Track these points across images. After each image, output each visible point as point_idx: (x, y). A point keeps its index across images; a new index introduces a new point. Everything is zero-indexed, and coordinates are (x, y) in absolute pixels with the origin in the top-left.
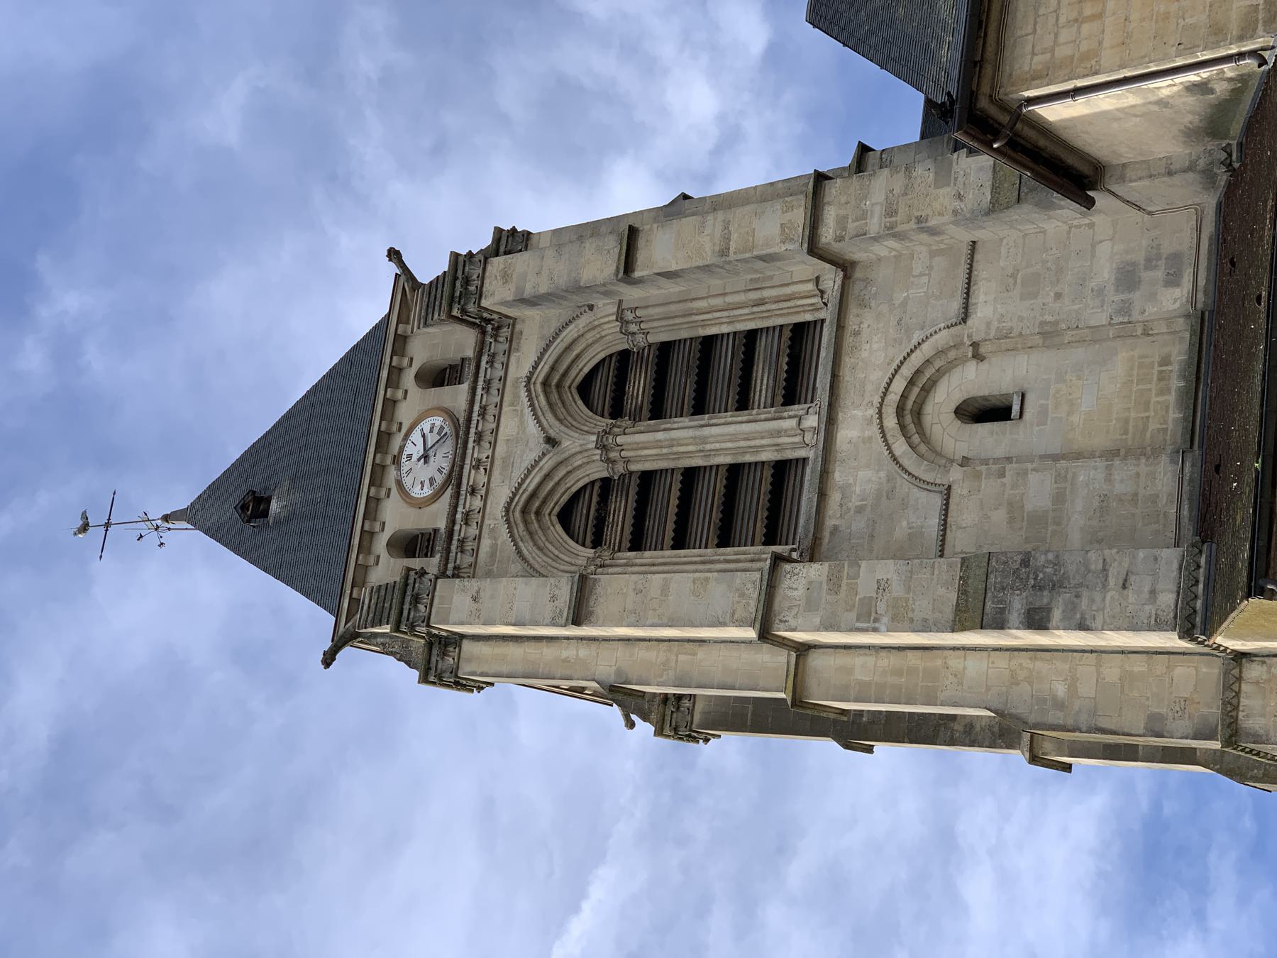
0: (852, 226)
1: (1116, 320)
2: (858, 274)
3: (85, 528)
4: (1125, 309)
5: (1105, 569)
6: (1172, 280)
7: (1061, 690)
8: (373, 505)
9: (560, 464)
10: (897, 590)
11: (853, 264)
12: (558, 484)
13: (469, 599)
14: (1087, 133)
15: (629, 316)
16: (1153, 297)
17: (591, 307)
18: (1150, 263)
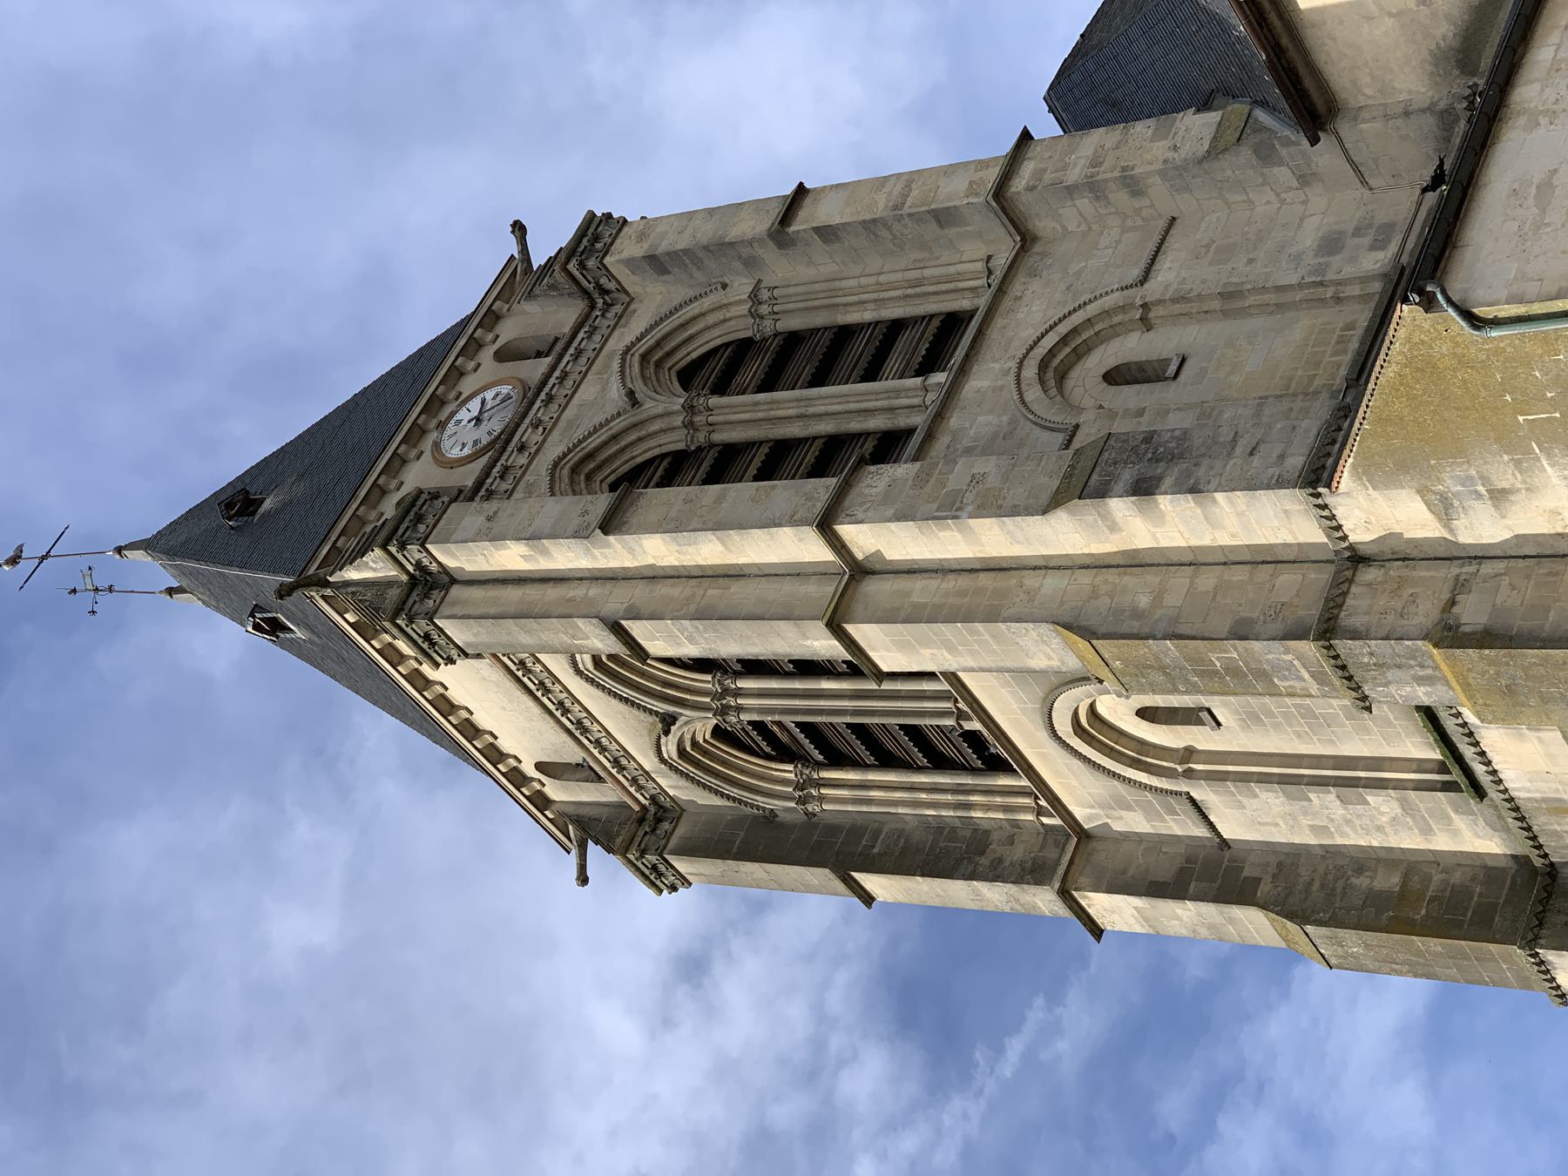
1: (1308, 280)
2: (1037, 248)
3: (14, 561)
5: (1234, 441)
7: (1144, 601)
8: (397, 463)
9: (635, 426)
11: (1035, 239)
12: (623, 450)
13: (482, 518)
14: (1334, 39)
16: (1353, 259)
17: (724, 286)
18: (1358, 232)
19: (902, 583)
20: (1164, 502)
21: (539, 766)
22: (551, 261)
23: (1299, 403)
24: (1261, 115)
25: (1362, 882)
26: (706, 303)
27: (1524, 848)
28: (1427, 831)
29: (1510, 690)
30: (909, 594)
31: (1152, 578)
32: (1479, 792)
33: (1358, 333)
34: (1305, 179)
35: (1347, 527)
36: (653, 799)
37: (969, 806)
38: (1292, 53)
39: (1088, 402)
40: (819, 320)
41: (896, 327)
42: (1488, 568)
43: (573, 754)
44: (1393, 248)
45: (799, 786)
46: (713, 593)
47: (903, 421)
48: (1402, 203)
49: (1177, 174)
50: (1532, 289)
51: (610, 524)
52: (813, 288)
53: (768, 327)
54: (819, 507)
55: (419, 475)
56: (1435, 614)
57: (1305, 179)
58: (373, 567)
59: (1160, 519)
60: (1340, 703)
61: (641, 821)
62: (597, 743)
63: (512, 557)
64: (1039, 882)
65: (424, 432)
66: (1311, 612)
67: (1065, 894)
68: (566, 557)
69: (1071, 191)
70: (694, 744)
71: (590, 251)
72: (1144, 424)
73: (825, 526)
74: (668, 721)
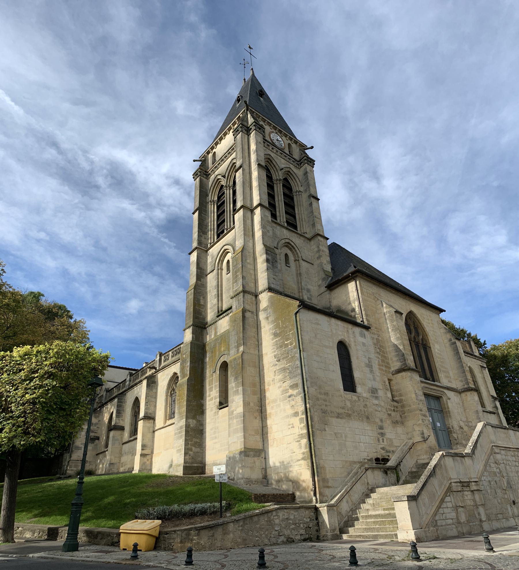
0: (321, 243)
2: (308, 241)
3: (250, 47)
4: (304, 289)
7: (248, 261)
15: (300, 193)
18: (310, 295)
19: (250, 218)
20: (265, 264)
21: (215, 152)
24: (330, 278)
25: (202, 298)
26: (299, 183)
28: (211, 308)
29: (235, 321)
31: (252, 262)
32: (218, 317)
33: (294, 295)
34: (319, 286)
36: (210, 174)
39: (282, 251)
40: (296, 203)
41: (295, 217)
42: (255, 317)
45: (213, 201)
47: (278, 218)
49: (321, 265)
51: (259, 165)
52: (301, 202)
53: (294, 194)
54: (263, 203)
55: (267, 129)
56: (247, 309)
58: (250, 120)
60: (232, 294)
61: (206, 172)
62: (220, 163)
63: (253, 147)
65: (275, 130)
66: (247, 289)
67: (196, 248)
68: (253, 157)
69: (318, 247)
71: (308, 161)
72: (278, 261)
73: (260, 205)
74: (224, 177)
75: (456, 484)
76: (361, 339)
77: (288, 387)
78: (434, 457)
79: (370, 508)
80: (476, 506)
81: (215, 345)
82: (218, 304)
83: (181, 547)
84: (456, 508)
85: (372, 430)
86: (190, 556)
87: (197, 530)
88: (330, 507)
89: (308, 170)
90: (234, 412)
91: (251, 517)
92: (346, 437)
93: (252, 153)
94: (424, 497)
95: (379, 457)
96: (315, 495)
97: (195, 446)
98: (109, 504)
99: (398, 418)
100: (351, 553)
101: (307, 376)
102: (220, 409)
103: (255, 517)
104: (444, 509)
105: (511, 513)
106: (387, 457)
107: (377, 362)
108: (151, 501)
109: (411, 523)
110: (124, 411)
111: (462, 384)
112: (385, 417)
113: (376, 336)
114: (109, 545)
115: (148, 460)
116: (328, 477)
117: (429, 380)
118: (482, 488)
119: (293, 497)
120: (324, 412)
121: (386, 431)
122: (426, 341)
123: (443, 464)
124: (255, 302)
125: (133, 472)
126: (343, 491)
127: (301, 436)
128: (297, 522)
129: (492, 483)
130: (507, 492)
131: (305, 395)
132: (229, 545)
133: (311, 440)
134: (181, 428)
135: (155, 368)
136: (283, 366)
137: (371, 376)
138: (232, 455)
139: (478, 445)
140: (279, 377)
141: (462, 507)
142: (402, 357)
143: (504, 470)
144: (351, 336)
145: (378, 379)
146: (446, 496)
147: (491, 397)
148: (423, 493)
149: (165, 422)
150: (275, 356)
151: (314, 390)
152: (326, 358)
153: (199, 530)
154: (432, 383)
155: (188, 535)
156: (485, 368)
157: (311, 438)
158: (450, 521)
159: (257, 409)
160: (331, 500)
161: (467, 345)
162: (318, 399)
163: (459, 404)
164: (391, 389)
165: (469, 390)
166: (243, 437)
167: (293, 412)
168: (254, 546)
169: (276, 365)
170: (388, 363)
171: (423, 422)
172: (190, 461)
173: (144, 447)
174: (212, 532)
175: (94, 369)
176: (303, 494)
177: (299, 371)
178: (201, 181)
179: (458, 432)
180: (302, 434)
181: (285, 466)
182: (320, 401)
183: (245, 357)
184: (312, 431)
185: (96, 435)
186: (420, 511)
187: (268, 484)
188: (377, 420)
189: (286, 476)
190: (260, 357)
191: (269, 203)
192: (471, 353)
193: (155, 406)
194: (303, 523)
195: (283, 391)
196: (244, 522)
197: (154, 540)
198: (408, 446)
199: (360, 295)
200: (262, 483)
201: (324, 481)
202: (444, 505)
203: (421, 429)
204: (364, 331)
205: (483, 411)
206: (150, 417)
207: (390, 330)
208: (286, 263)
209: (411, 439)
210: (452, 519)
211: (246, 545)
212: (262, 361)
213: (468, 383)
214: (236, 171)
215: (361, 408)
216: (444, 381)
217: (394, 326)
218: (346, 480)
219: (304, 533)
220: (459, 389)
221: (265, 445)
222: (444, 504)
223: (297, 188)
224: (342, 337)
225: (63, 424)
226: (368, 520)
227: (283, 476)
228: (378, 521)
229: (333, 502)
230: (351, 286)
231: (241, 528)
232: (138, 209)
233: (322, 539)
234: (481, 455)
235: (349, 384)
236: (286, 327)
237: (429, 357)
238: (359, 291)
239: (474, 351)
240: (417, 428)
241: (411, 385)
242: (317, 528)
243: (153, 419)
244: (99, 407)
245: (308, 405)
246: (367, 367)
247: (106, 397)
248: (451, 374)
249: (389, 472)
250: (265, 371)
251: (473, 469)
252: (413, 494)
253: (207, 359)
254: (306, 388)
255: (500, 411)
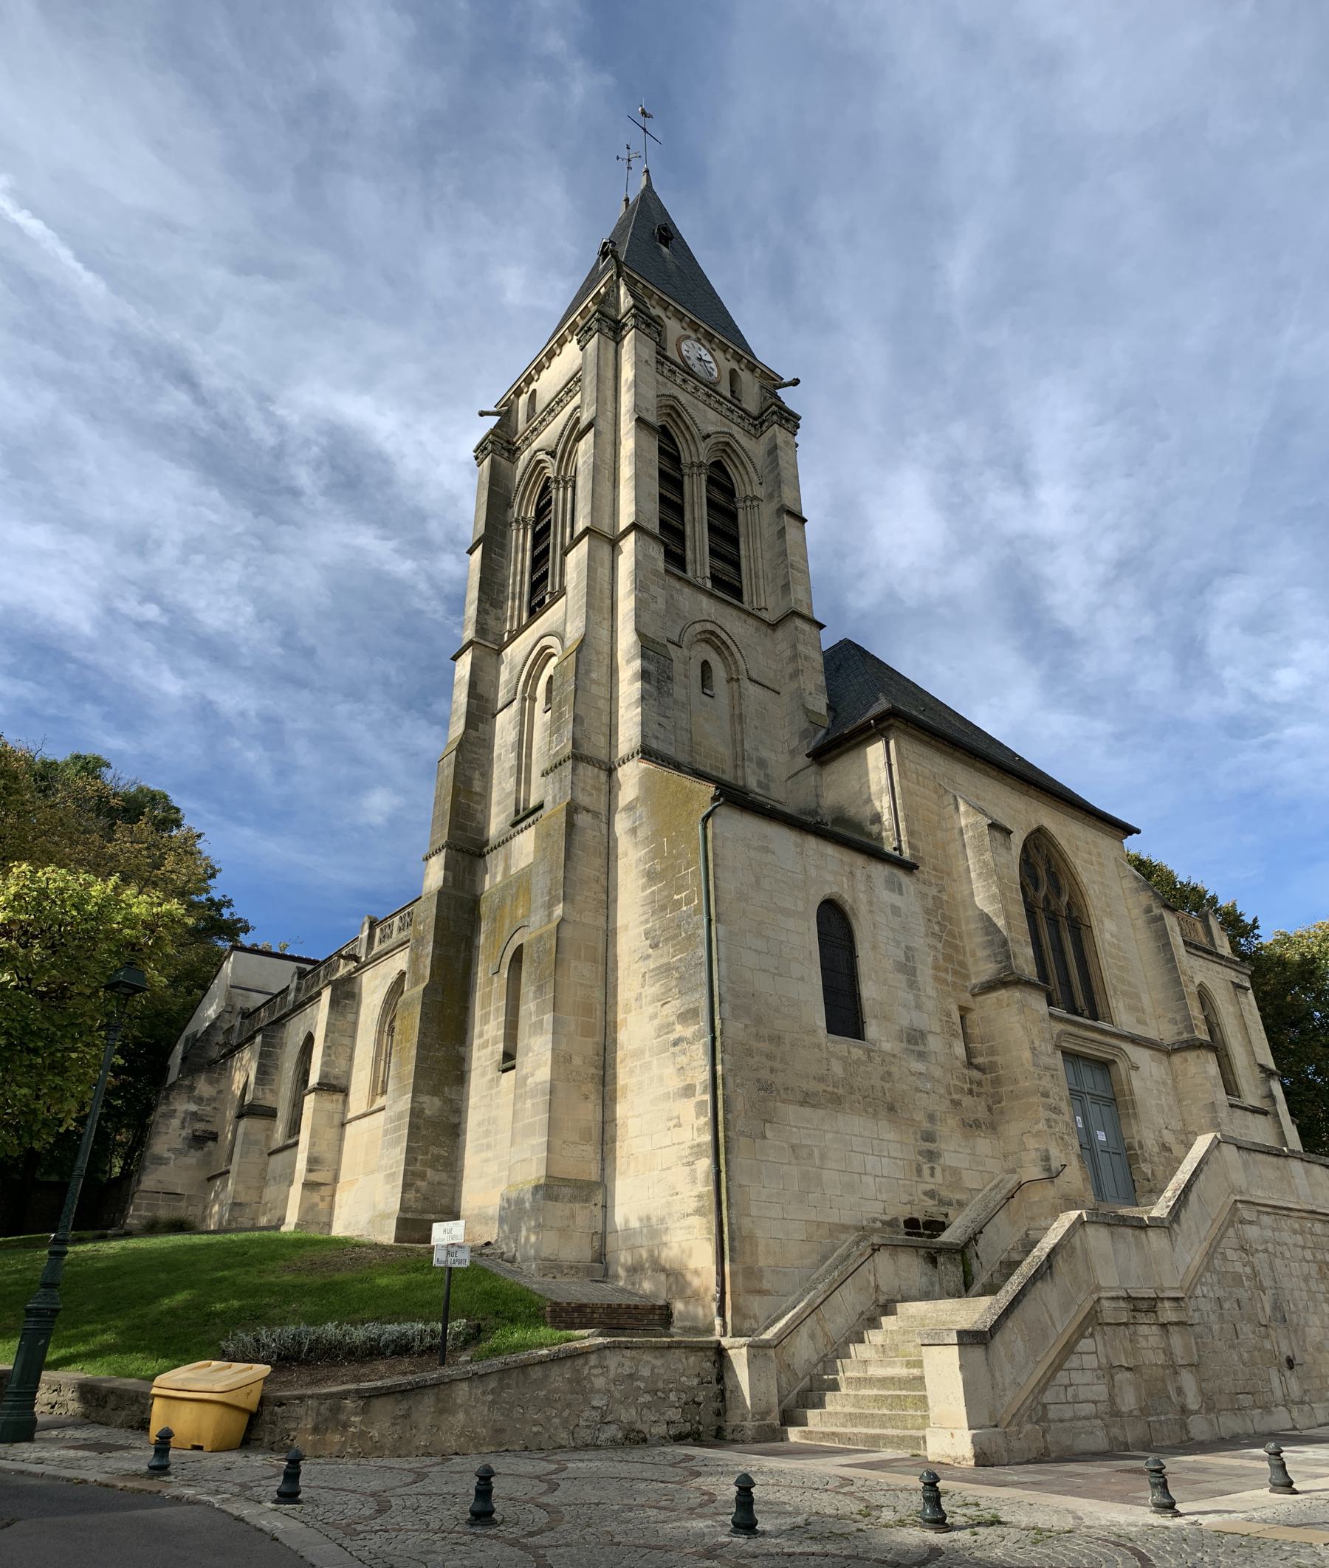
3: (644, 113)
4: (750, 759)
6: (759, 784)
7: (594, 675)
10: (653, 606)
15: (755, 503)
18: (766, 775)
19: (607, 564)
20: (638, 685)
21: (534, 391)
22: (779, 398)
23: (687, 748)
24: (823, 732)
25: (477, 775)
26: (753, 475)
27: (491, 844)
28: (499, 803)
29: (549, 835)
30: (602, 566)
31: (605, 679)
32: (514, 825)
33: (720, 775)
34: (793, 753)
35: (624, 767)
36: (519, 448)
37: (513, 600)
38: (848, 745)
39: (693, 653)
40: (742, 530)
41: (737, 566)
42: (604, 827)
43: (539, 408)
44: (758, 790)
45: (524, 519)
46: (607, 473)
47: (689, 567)
48: (782, 795)
49: (799, 694)
50: (719, 843)
51: (640, 421)
52: (756, 526)
53: (741, 504)
54: (644, 524)
55: (673, 328)
56: (583, 804)
57: (793, 753)
58: (625, 301)
59: (631, 683)
60: (547, 765)
61: (508, 442)
62: (544, 420)
63: (627, 373)
64: (477, 631)
65: (696, 331)
66: (585, 750)
67: (471, 643)
68: (626, 400)
69: (794, 647)
70: (544, 468)
71: (782, 417)
72: (677, 678)
73: (634, 527)
74: (552, 454)
75: (1113, 1304)
76: (887, 897)
77: (673, 1018)
78: (1055, 1225)
79: (870, 1359)
80: (1174, 1369)
81: (502, 901)
82: (518, 791)
83: (314, 1444)
84: (1110, 1371)
85: (902, 1143)
86: (292, 1474)
87: (361, 1398)
88: (757, 1350)
89: (780, 441)
90: (530, 1081)
91: (524, 1367)
92: (823, 1157)
93: (624, 389)
94: (1013, 1334)
95: (916, 1215)
96: (721, 1312)
97: (433, 1167)
98: (172, 1312)
99: (981, 1113)
100: (738, 1494)
101: (724, 989)
102: (504, 1071)
103: (537, 1368)
104: (1073, 1374)
105: (1278, 1393)
106: (941, 1219)
107: (930, 959)
108: (277, 1311)
109: (964, 1410)
110: (276, 1067)
111: (1175, 1029)
112: (942, 1107)
113: (934, 891)
114: (131, 1427)
115: (322, 1199)
116: (762, 1263)
117: (1081, 1015)
118: (1196, 1318)
119: (664, 1315)
120: (766, 1088)
121: (943, 1146)
122: (1080, 911)
123: (1078, 1244)
124: (605, 788)
125: (283, 1229)
126: (802, 1304)
127: (697, 1150)
128: (661, 1385)
129: (1227, 1305)
130: (1272, 1333)
131: (714, 1039)
132: (452, 1443)
133: (722, 1162)
134: (400, 1116)
135: (356, 959)
136: (664, 961)
137: (911, 997)
138: (514, 1195)
139: (1193, 1197)
140: (654, 990)
141: (1128, 1369)
142: (1001, 947)
143: (1267, 1270)
144: (862, 887)
145: (930, 1005)
146: (1082, 1336)
147: (1257, 1070)
148: (1010, 1324)
149: (372, 1102)
150: (647, 934)
151: (741, 1026)
152: (782, 942)
153: (368, 1397)
154: (1089, 1022)
155: (336, 1410)
156: (1247, 989)
157: (722, 1157)
158: (1088, 1409)
159: (592, 1075)
160: (767, 1328)
161: (1199, 925)
162: (749, 1053)
163: (1164, 1083)
164: (965, 1033)
165: (1200, 1046)
166: (545, 1146)
167: (682, 1084)
168: (526, 1449)
169: (649, 956)
170: (963, 964)
171: (1050, 1127)
172: (419, 1206)
173: (313, 1163)
174: (405, 1405)
175: (133, 946)
176: (691, 1308)
177: (704, 975)
178: (494, 465)
179: (1156, 1159)
180: (699, 1145)
181: (654, 1229)
182: (757, 1059)
183: (568, 932)
184: (725, 1136)
185: (211, 1128)
186: (997, 1374)
187: (606, 1275)
188: (920, 1116)
189: (652, 1256)
190: (609, 935)
191: (663, 524)
192: (1209, 947)
193: (351, 1058)
194: (677, 1390)
195: (661, 1027)
196: (501, 1380)
197: (244, 1419)
198: (1004, 1192)
199: (896, 777)
200: (589, 1272)
201: (751, 1273)
202: (1074, 1362)
203: (1042, 1147)
204: (900, 875)
205: (1232, 1106)
206: (335, 1087)
207: (973, 875)
208: (703, 687)
209: (1013, 1171)
210: (1095, 1402)
211: (502, 1445)
212: (615, 946)
213: (1190, 1028)
214: (578, 439)
215: (872, 1082)
216: (1125, 1020)
217: (985, 864)
218: (815, 1276)
219: (677, 1418)
220: (1165, 1042)
221: (608, 1171)
222: (1074, 1357)
223: (749, 489)
224: (835, 889)
225: (25, 1091)
226: (863, 1392)
227: (645, 1255)
228: (887, 1397)
229: (768, 1335)
230: (875, 753)
231: (490, 1398)
232: (397, 551)
233: (729, 1437)
234: (1197, 1226)
235: (845, 1014)
236: (680, 855)
237: (1087, 952)
238: (895, 768)
239: (1218, 942)
240: (1032, 1143)
241: (1024, 1029)
242: (716, 1405)
243: (344, 1091)
244: (224, 1056)
245: (719, 1068)
246: (899, 971)
247: (241, 1030)
248: (1146, 1001)
249: (941, 1260)
250: (620, 973)
251: (1172, 1264)
252: (980, 1326)
253: (482, 937)
254: (717, 1022)
255: (1282, 1108)
